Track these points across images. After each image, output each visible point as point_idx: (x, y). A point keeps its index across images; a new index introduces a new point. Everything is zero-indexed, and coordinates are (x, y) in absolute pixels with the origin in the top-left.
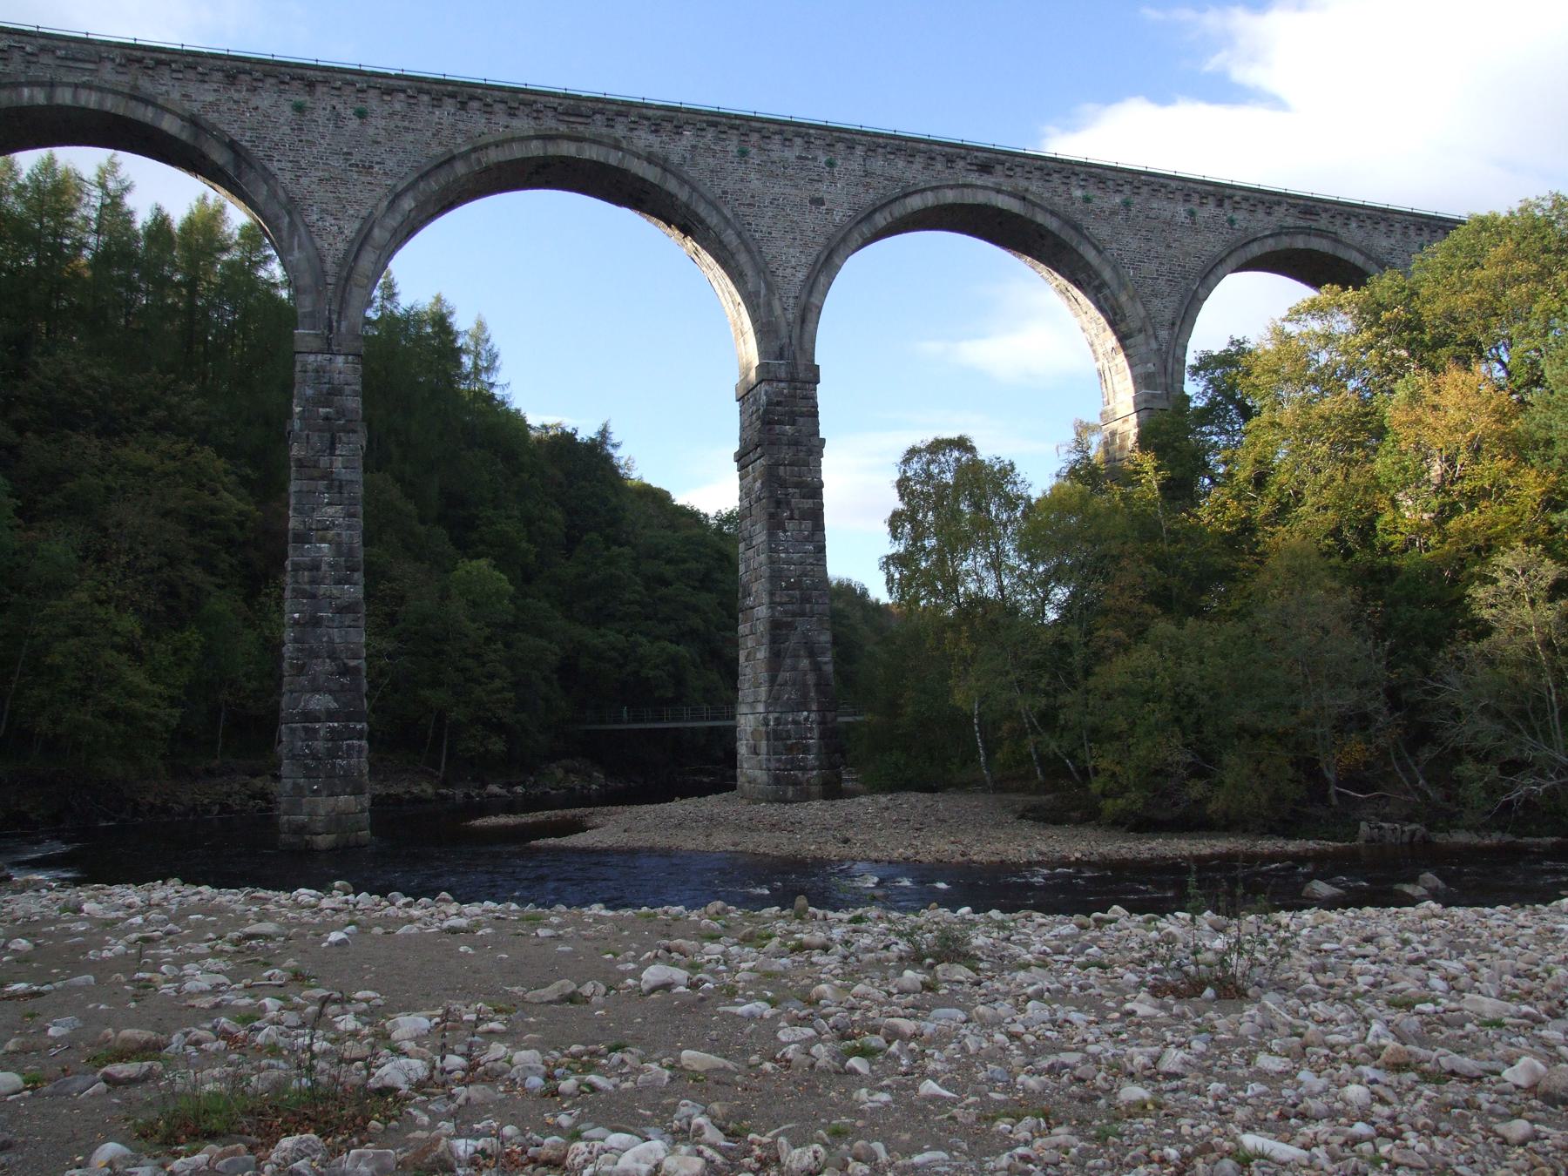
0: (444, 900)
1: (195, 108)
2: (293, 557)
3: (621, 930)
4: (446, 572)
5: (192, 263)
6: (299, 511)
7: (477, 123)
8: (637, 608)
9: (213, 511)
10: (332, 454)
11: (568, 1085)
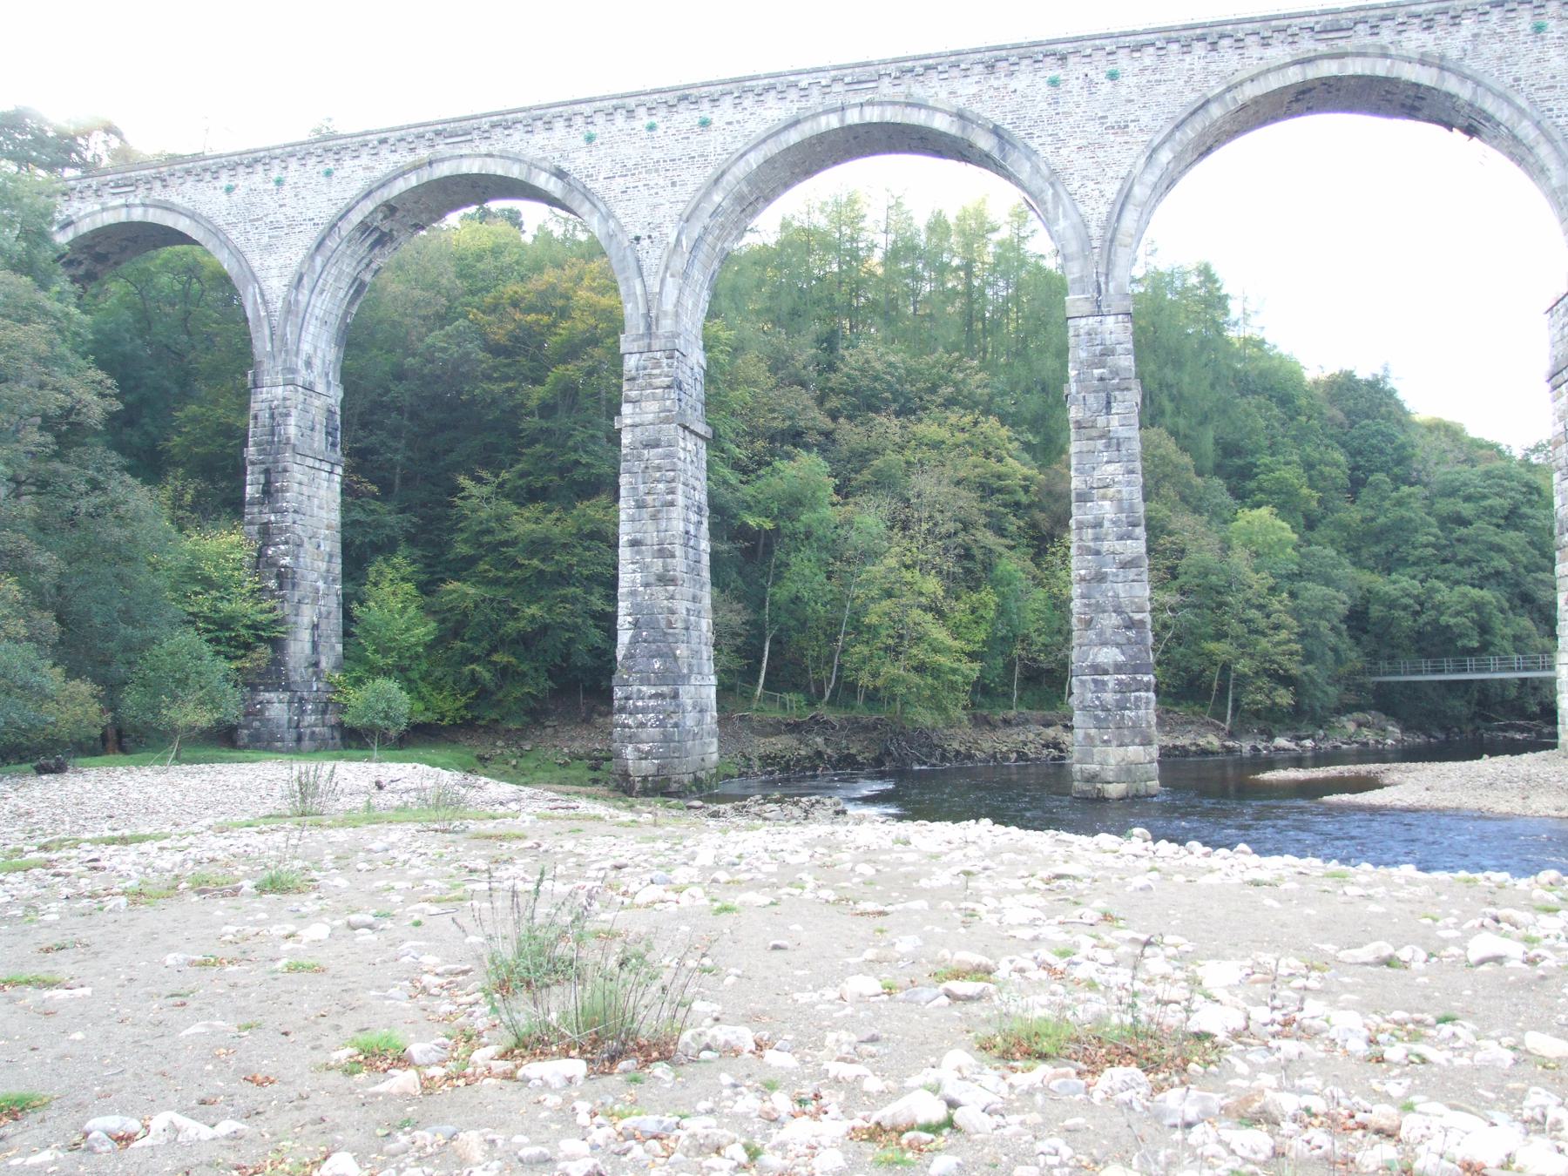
0: (1243, 852)
1: (960, 102)
2: (1078, 514)
3: (1438, 894)
4: (1225, 522)
5: (968, 246)
6: (1080, 471)
7: (1229, 61)
8: (1430, 551)
9: (1000, 477)
10: (1108, 413)
11: (1395, 1052)
